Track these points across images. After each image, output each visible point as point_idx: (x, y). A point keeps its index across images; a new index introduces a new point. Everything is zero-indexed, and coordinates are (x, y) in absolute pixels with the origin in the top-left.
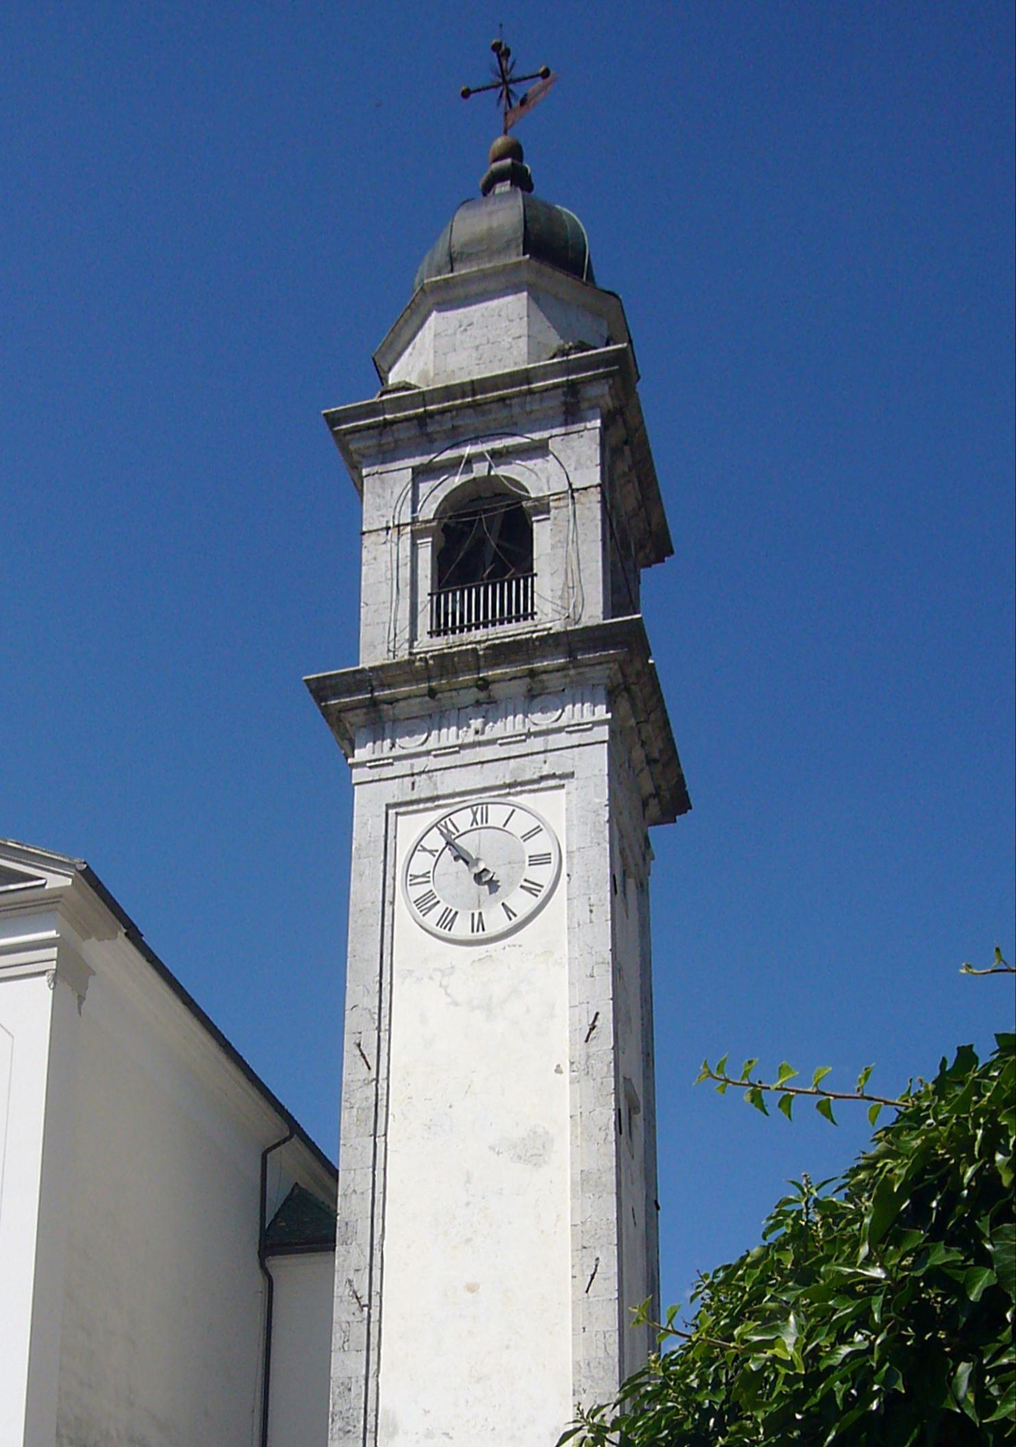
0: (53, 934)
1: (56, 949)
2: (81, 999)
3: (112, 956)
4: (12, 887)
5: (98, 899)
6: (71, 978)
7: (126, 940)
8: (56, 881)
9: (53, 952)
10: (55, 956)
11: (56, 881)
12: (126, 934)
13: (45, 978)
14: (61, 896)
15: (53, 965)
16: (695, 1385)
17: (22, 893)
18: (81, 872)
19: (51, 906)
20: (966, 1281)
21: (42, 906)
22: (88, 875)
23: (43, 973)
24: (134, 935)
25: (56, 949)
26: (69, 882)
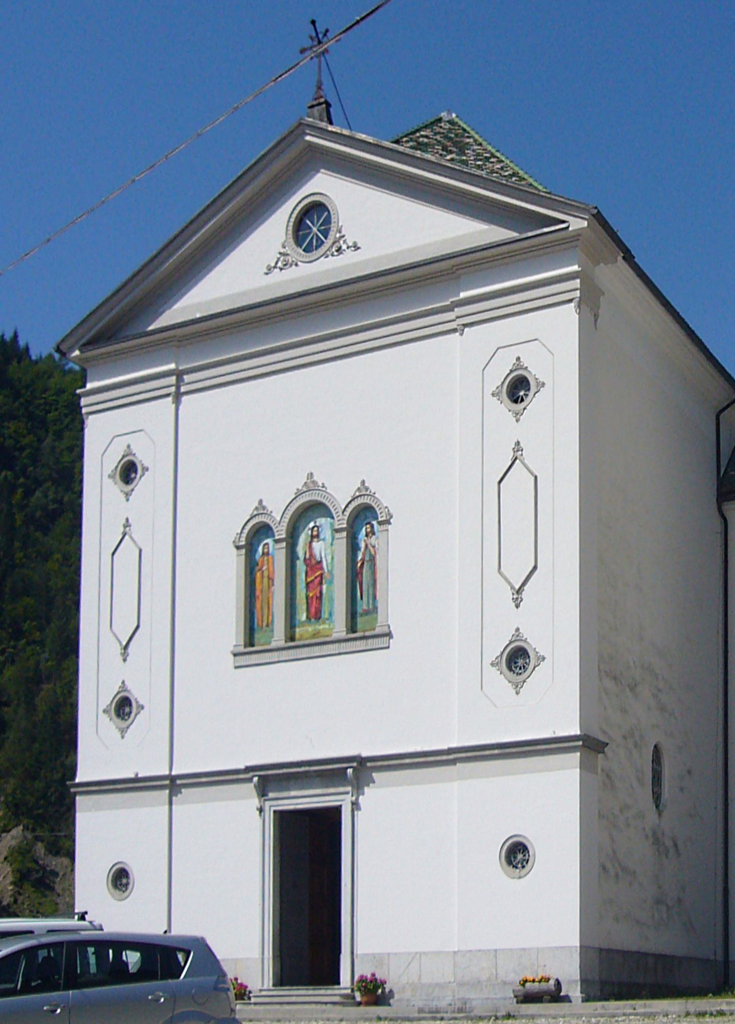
0: (575, 268)
1: (578, 281)
2: (596, 317)
3: (615, 276)
4: (530, 234)
5: (606, 235)
6: (590, 303)
7: (623, 261)
8: (577, 224)
9: (577, 283)
10: (579, 286)
11: (577, 224)
12: (624, 258)
13: (572, 305)
14: (579, 235)
15: (578, 293)
16: (133, 968)
17: (554, 235)
18: (593, 215)
19: (573, 244)
20: (70, 886)
21: (568, 243)
22: (599, 218)
23: (570, 301)
24: (629, 258)
25: (578, 281)
26: (585, 224)
